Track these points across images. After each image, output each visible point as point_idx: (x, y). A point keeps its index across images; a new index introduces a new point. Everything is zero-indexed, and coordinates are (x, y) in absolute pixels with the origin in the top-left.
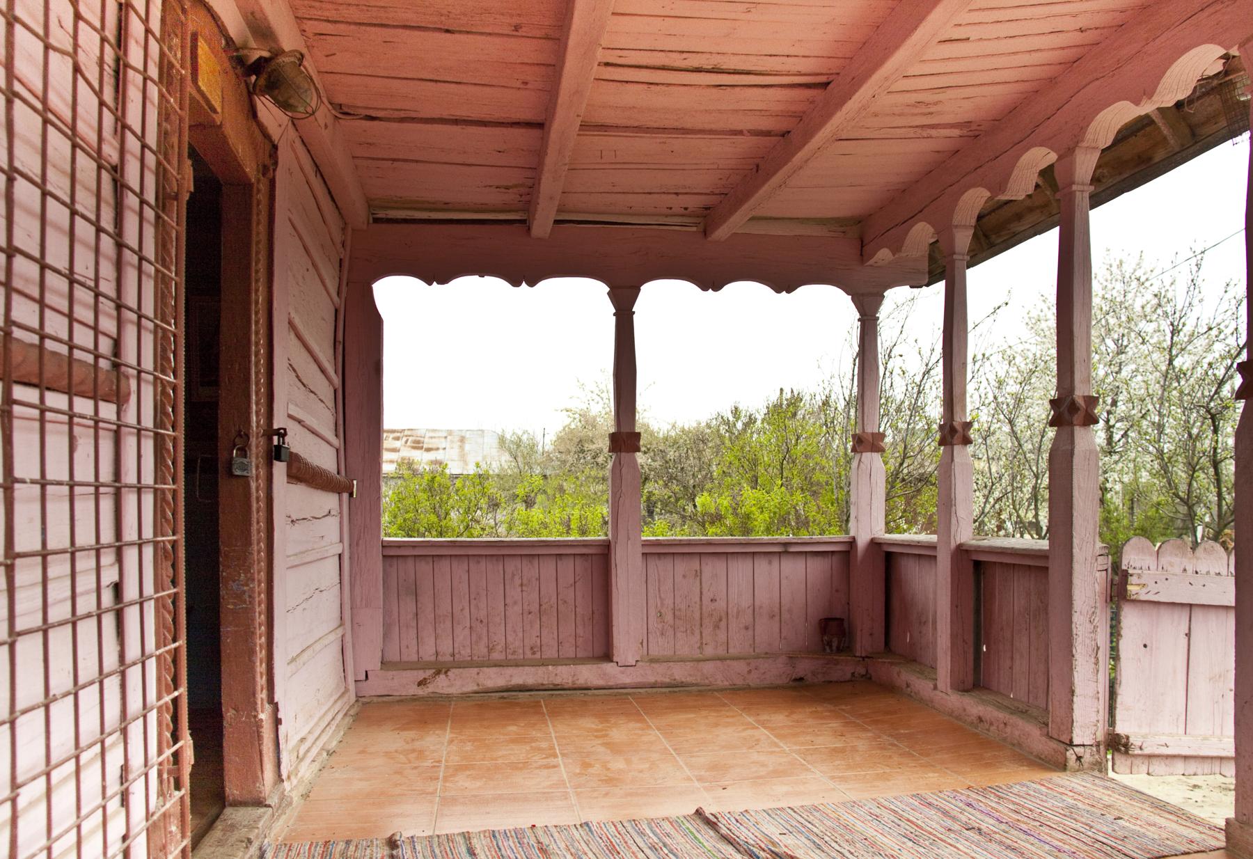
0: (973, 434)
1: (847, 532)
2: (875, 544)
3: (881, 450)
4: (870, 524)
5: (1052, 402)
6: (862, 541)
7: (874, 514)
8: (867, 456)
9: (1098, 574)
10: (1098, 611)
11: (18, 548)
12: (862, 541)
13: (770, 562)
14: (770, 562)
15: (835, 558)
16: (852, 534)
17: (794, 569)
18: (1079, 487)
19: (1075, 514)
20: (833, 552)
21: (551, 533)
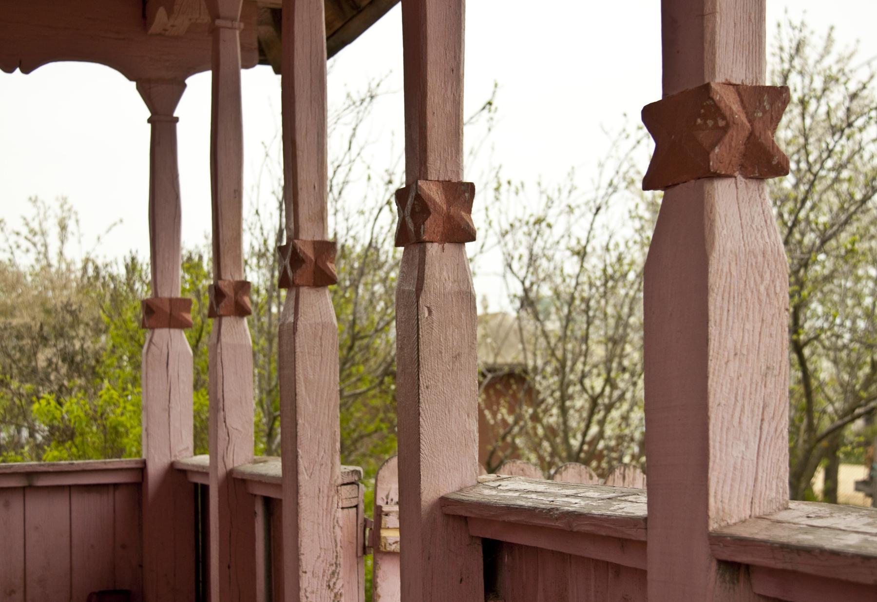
0: (339, 269)
1: (140, 456)
2: (176, 473)
3: (183, 325)
4: (169, 444)
5: (650, 114)
6: (156, 466)
7: (175, 423)
8: (162, 334)
9: (340, 514)
10: (342, 571)
11: (355, 509)
12: (156, 466)
13: (7, 505)
14: (7, 505)
15: (120, 495)
16: (144, 457)
17: (49, 516)
18: (306, 379)
19: (300, 421)
20: (116, 486)
21: (23, 459)
